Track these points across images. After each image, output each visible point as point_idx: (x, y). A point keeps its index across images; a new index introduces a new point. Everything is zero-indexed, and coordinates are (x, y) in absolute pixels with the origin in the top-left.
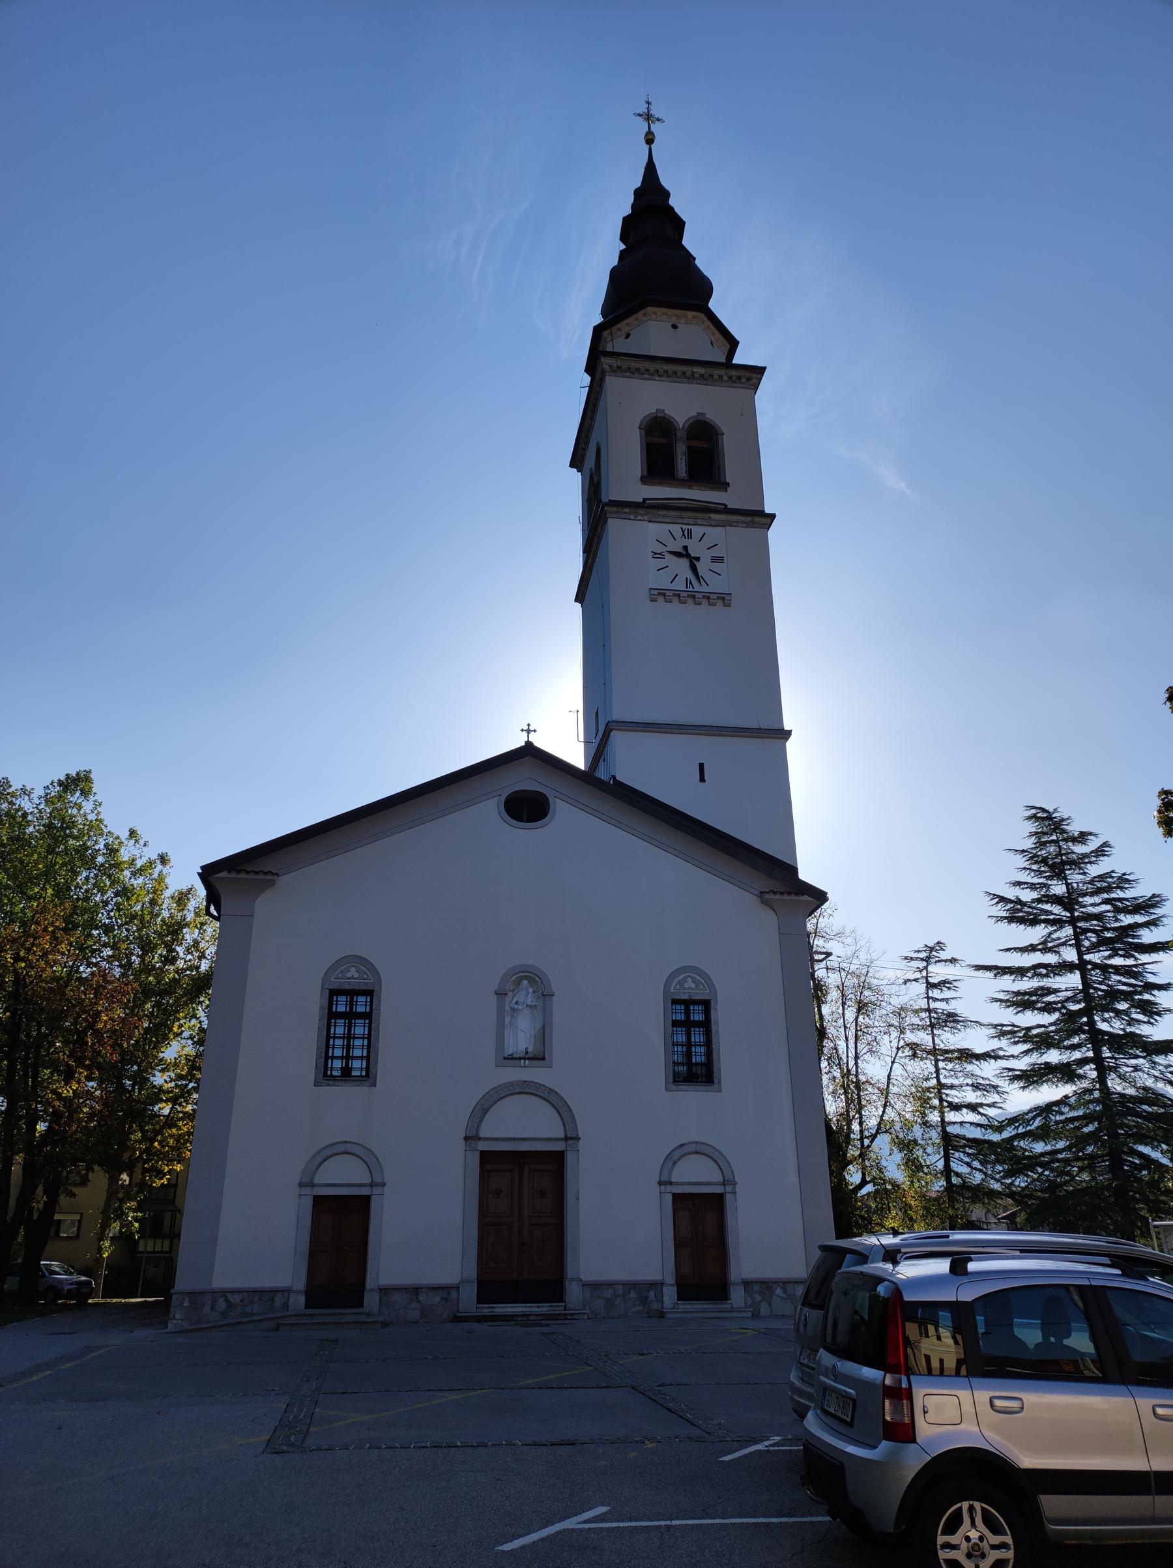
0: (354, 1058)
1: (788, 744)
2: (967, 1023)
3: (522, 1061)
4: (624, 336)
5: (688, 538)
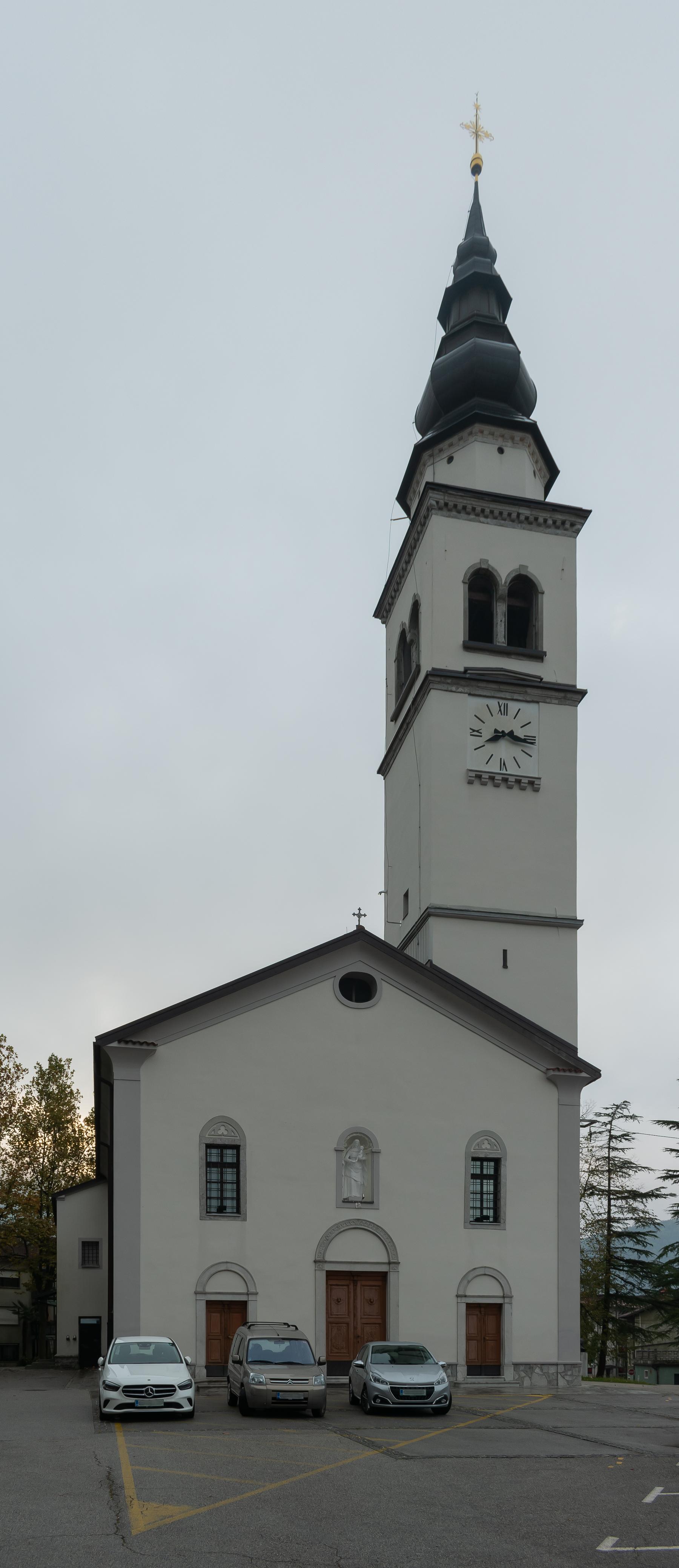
0: (226, 1198)
1: (578, 931)
2: (637, 1168)
3: (356, 1204)
4: (446, 460)
5: (504, 715)
